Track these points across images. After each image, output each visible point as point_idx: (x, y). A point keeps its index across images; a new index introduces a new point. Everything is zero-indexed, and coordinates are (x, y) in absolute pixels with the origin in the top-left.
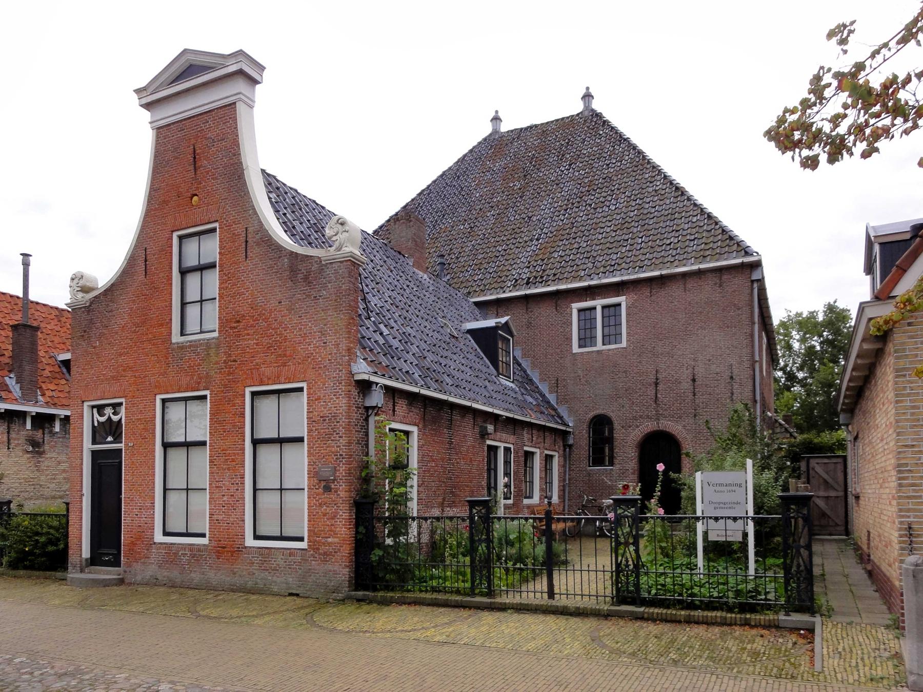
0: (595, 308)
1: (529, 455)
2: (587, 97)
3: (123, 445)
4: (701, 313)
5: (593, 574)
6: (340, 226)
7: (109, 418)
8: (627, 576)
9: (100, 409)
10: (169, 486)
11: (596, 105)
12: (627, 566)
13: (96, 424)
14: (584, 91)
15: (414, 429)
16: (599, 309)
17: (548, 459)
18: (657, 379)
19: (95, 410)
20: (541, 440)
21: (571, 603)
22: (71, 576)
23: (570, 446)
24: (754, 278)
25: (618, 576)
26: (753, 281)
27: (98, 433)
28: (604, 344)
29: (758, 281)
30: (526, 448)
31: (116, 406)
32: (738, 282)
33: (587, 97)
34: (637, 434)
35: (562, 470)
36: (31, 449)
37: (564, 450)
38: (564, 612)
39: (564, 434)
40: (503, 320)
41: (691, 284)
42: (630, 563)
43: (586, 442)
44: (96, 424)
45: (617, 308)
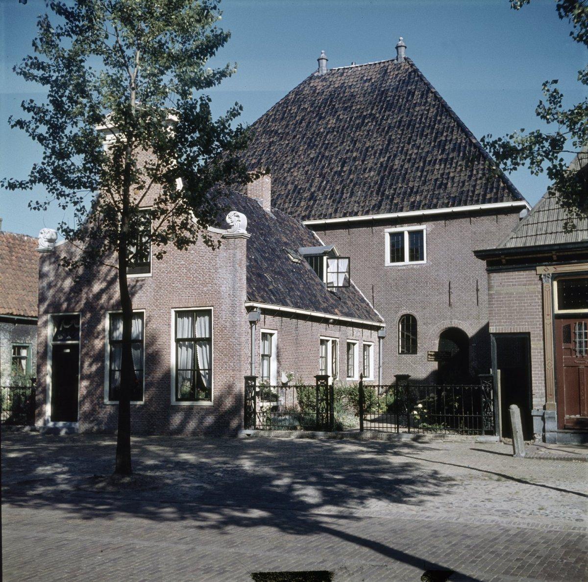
4: (483, 240)
17: (366, 347)
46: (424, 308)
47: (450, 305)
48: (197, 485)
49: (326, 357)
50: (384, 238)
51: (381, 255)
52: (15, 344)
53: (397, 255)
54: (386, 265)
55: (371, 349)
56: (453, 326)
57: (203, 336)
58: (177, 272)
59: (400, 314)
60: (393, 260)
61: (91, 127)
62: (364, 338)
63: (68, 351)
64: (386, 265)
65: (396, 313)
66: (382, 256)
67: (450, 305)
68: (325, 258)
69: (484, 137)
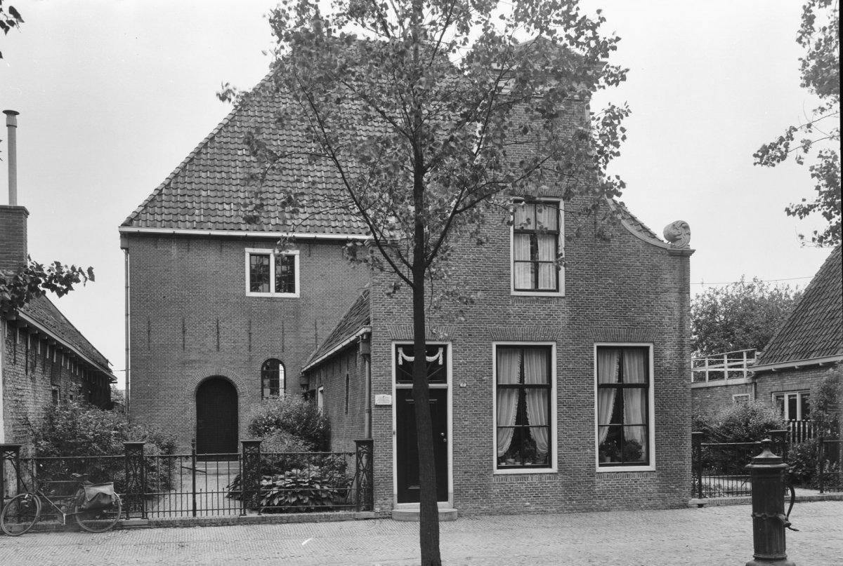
5: (210, 507)
19: (400, 351)
44: (401, 362)
49: (498, 427)
58: (601, 294)
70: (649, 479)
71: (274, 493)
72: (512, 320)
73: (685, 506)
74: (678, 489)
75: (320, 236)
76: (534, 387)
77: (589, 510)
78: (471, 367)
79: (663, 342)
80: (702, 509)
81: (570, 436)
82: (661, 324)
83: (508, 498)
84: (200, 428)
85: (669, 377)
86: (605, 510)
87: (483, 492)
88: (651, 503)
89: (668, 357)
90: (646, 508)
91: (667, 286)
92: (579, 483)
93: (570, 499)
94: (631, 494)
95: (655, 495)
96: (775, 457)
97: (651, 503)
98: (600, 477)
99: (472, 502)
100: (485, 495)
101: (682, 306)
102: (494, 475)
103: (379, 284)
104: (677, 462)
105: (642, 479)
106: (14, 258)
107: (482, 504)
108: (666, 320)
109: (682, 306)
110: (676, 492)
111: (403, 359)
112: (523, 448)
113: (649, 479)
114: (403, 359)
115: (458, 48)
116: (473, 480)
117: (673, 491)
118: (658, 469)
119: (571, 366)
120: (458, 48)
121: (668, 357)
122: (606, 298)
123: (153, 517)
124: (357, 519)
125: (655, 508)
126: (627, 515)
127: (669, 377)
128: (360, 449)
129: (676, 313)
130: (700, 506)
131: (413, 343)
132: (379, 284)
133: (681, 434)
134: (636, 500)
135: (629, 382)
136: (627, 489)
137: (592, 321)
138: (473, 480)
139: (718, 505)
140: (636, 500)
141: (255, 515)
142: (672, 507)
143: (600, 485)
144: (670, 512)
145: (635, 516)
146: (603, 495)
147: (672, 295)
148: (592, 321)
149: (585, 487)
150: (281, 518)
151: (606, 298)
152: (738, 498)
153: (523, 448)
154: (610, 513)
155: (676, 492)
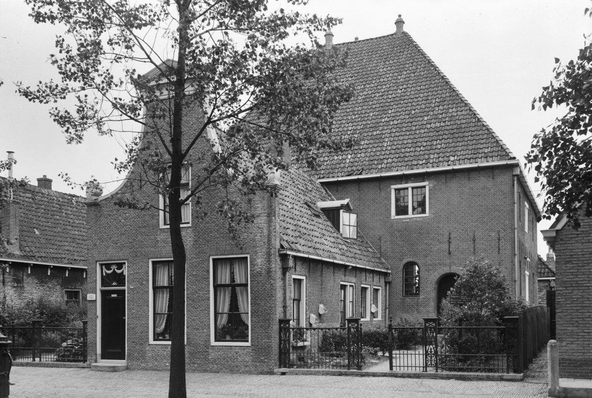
0: (407, 188)
1: (364, 290)
2: (399, 23)
3: (126, 288)
4: (479, 195)
5: (410, 365)
6: (269, 170)
7: (114, 270)
8: (431, 357)
9: (108, 266)
10: (156, 312)
11: (406, 28)
12: (431, 352)
13: (104, 274)
14: (397, 17)
15: (304, 278)
16: (410, 190)
17: (376, 291)
18: (450, 238)
19: (104, 267)
20: (371, 279)
21: (403, 370)
22: (517, 299)
23: (390, 283)
24: (514, 173)
25: (426, 357)
26: (514, 176)
27: (105, 281)
28: (413, 214)
29: (517, 175)
30: (363, 286)
31: (120, 266)
32: (504, 179)
33: (399, 23)
34: (435, 276)
35: (384, 299)
36: (16, 285)
37: (386, 286)
38: (396, 376)
39: (386, 275)
40: (345, 202)
41: (473, 175)
42: (433, 350)
43: (401, 279)
44: (104, 274)
45: (423, 189)
46: (426, 257)
47: (450, 253)
48: (549, 373)
49: (155, 314)
50: (390, 194)
51: (388, 209)
52: (67, 290)
53: (402, 210)
54: (392, 218)
55: (380, 293)
56: (452, 272)
57: (223, 283)
58: (214, 222)
59: (405, 261)
60: (398, 213)
61: (218, 72)
62: (374, 283)
63: (115, 296)
64: (392, 218)
65: (401, 261)
66: (389, 210)
67: (450, 253)
68: (341, 211)
69: (45, 103)
70: (245, 351)
71: (291, 355)
72: (159, 244)
73: (271, 373)
74: (266, 360)
75: (383, 174)
76: (240, 285)
77: (205, 371)
78: (137, 276)
79: (256, 252)
80: (284, 376)
81: (194, 320)
82: (254, 241)
83: (156, 360)
84: (254, 308)
85: (260, 279)
86: (216, 372)
87: (142, 356)
88: (247, 369)
89: (260, 264)
90: (244, 372)
91: (259, 212)
92: (199, 352)
93: (194, 363)
94: (233, 362)
95: (250, 363)
96: (4, 336)
97: (247, 369)
98: (213, 349)
99: (136, 361)
100: (143, 357)
101: (269, 226)
102: (149, 345)
103: (90, 228)
104: (266, 341)
105: (241, 352)
106: (6, 226)
107: (142, 363)
108: (258, 237)
109: (269, 226)
110: (265, 362)
111: (106, 272)
112: (233, 328)
113: (245, 351)
114: (106, 272)
115: (69, 92)
116: (137, 347)
117: (262, 361)
118: (252, 345)
119: (194, 273)
120: (69, 92)
121: (260, 264)
122: (217, 225)
123: (364, 371)
124: (78, 367)
125: (250, 373)
126: (229, 377)
127: (260, 279)
128: (427, 324)
129: (265, 231)
130: (283, 374)
131: (172, 259)
132: (90, 228)
133: (269, 320)
134: (237, 367)
135: (239, 282)
136: (231, 358)
137: (208, 241)
138: (137, 347)
139: (297, 374)
140: (237, 367)
141: (445, 373)
142: (261, 373)
143: (212, 355)
144: (262, 377)
145: (207, 376)
146: (214, 361)
147: (262, 218)
148: (208, 241)
149: (203, 355)
150: (493, 376)
151: (217, 225)
152: (341, 370)
153: (233, 328)
154: (218, 374)
155: (265, 362)
